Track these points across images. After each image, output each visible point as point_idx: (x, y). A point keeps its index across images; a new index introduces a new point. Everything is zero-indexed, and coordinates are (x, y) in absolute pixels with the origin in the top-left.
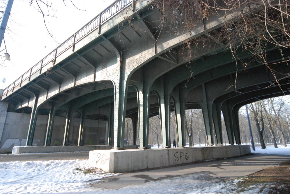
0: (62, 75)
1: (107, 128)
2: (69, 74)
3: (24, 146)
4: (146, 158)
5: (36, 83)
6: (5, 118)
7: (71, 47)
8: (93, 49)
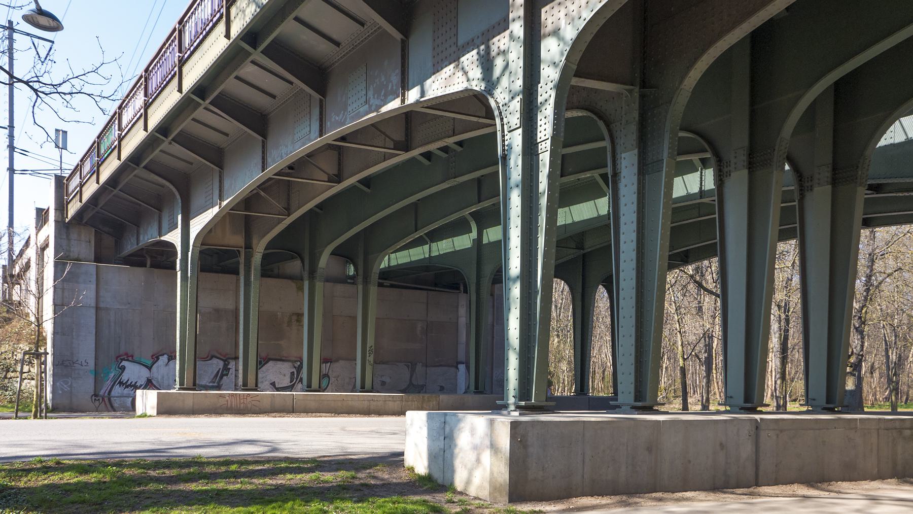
0: (150, 182)
1: (463, 320)
2: (291, 83)
3: (172, 391)
4: (649, 449)
5: (170, 138)
6: (93, 286)
7: (138, 119)
8: (194, 120)
